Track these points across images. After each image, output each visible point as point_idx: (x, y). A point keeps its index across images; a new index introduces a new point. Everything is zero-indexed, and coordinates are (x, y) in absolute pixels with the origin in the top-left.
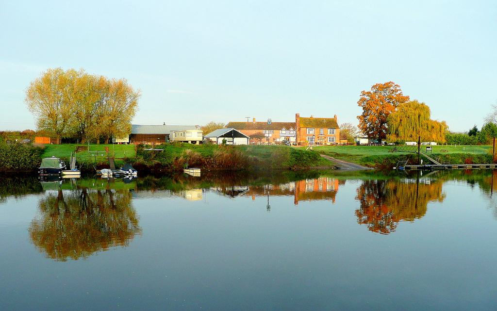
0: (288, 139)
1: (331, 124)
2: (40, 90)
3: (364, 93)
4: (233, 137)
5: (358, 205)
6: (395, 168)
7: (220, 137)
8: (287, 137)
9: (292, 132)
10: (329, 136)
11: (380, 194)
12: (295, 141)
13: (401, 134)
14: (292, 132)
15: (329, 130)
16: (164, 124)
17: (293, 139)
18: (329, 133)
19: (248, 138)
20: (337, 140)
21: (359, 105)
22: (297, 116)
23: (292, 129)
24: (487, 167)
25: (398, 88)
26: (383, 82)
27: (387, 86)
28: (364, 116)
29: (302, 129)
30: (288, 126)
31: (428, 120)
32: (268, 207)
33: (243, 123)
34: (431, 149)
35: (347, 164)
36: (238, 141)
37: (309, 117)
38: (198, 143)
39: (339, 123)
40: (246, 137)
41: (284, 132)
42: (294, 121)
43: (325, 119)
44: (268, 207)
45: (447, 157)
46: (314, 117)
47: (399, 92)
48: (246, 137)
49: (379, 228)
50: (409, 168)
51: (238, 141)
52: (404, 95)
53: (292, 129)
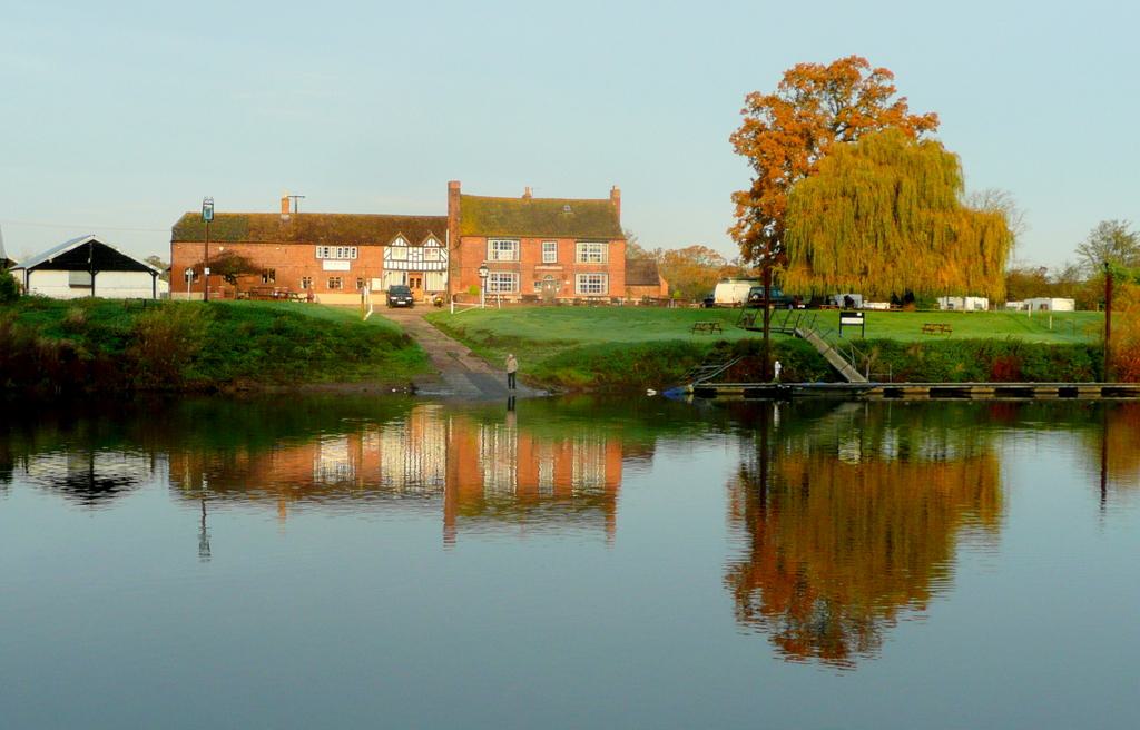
0: (416, 278)
1: (597, 221)
2: (1117, 234)
3: (757, 102)
4: (94, 269)
5: (734, 545)
7: (45, 266)
8: (412, 272)
9: (431, 260)
11: (504, 507)
12: (443, 288)
13: (824, 261)
14: (434, 256)
17: (436, 283)
19: (155, 274)
20: (609, 288)
21: (731, 140)
22: (453, 191)
23: (431, 242)
24: (1063, 392)
25: (886, 83)
26: (825, 58)
27: (840, 77)
28: (756, 193)
29: (468, 243)
30: (416, 230)
31: (948, 206)
32: (204, 545)
33: (238, 216)
34: (860, 321)
35: (731, 394)
36: (112, 286)
37: (518, 194)
43: (572, 203)
44: (204, 545)
45: (911, 352)
46: (537, 194)
47: (891, 101)
49: (833, 648)
50: (710, 393)
51: (112, 286)
52: (916, 109)
53: (431, 242)
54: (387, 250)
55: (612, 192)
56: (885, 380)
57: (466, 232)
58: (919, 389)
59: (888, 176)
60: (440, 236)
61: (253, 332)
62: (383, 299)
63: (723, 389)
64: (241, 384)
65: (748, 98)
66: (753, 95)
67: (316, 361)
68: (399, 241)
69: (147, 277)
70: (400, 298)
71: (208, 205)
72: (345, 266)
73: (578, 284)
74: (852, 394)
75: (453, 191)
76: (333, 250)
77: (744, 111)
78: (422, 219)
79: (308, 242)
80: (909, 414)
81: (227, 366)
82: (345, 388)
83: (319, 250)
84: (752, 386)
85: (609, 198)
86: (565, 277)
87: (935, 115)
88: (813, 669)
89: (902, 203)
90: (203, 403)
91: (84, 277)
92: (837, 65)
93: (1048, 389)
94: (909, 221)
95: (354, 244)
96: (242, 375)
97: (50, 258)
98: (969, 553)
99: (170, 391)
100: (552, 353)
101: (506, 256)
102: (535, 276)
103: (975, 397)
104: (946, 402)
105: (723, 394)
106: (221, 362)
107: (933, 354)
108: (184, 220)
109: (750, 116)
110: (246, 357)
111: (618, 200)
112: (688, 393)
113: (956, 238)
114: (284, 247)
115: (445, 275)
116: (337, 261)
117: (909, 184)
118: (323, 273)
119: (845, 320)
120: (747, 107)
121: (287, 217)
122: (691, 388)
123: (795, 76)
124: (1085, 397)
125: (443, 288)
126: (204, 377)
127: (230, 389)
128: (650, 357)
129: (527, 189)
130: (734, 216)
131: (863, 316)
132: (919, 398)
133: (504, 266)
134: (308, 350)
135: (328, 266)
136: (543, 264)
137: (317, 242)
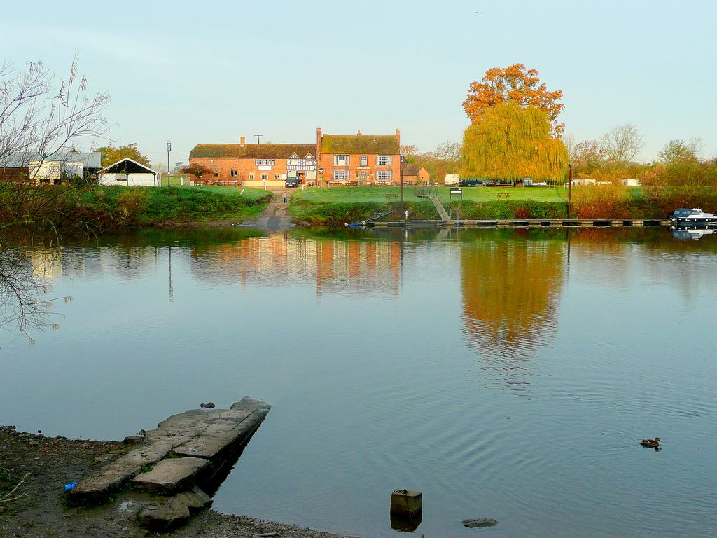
1: (387, 146)
3: (476, 87)
6: (346, 225)
9: (309, 164)
10: (379, 169)
12: (315, 178)
14: (310, 163)
15: (378, 158)
16: (74, 151)
18: (378, 163)
19: (155, 174)
22: (319, 133)
23: (309, 157)
24: (543, 224)
26: (504, 65)
27: (513, 73)
35: (381, 225)
36: (135, 180)
37: (355, 133)
38: (52, 183)
39: (403, 143)
40: (152, 173)
41: (294, 162)
42: (314, 142)
43: (376, 137)
46: (364, 133)
47: (538, 85)
48: (152, 173)
50: (372, 225)
52: (551, 90)
54: (288, 161)
56: (541, 217)
57: (323, 152)
58: (472, 223)
59: (504, 123)
60: (313, 154)
61: (179, 200)
62: (283, 184)
63: (378, 223)
64: (167, 222)
65: (471, 85)
66: (473, 83)
67: (205, 213)
70: (294, 183)
72: (269, 168)
73: (378, 175)
74: (444, 225)
76: (264, 161)
77: (469, 91)
78: (306, 146)
79: (252, 158)
80: (525, 233)
81: (162, 215)
82: (214, 224)
83: (257, 161)
84: (646, 220)
85: (395, 134)
86: (371, 172)
87: (560, 92)
90: (150, 230)
91: (123, 176)
92: (511, 69)
93: (557, 223)
94: (515, 144)
95: (273, 158)
96: (169, 218)
99: (133, 225)
100: (315, 208)
101: (342, 163)
102: (357, 172)
103: (499, 226)
104: (568, 228)
105: (377, 225)
106: (160, 213)
107: (487, 207)
108: (195, 148)
109: (472, 93)
110: (173, 211)
111: (399, 136)
112: (362, 225)
113: (536, 153)
114: (240, 160)
115: (316, 172)
116: (265, 167)
117: (514, 127)
118: (259, 172)
119: (452, 192)
120: (470, 89)
121: (243, 146)
122: (364, 223)
123: (491, 74)
124: (554, 226)
125: (315, 178)
126: (149, 219)
127: (161, 225)
128: (355, 209)
129: (359, 131)
130: (563, 125)
131: (461, 190)
132: (472, 227)
133: (341, 167)
134: (203, 208)
135: (261, 168)
136: (360, 166)
137: (256, 157)
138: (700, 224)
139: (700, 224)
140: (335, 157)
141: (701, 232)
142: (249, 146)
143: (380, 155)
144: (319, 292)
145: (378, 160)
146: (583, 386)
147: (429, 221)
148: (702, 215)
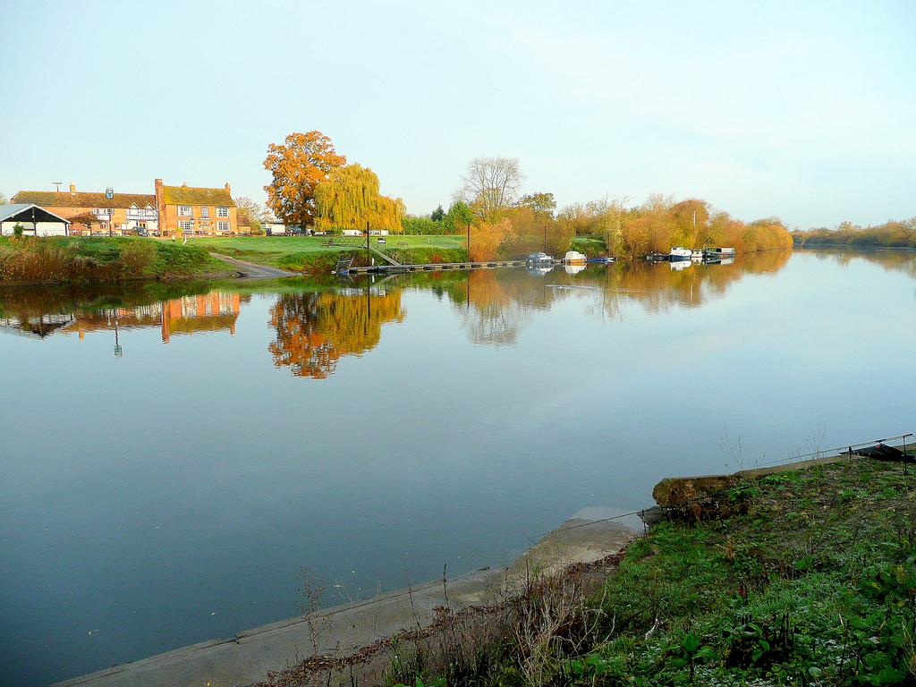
1: (221, 198)
3: (273, 148)
4: (35, 221)
8: (140, 221)
9: (149, 213)
10: (219, 219)
11: (308, 315)
13: (338, 218)
14: (150, 213)
15: (218, 210)
18: (218, 214)
22: (158, 183)
24: (461, 267)
25: (328, 143)
27: (309, 138)
30: (141, 202)
31: (376, 195)
36: (44, 229)
37: (179, 184)
47: (329, 149)
55: (226, 186)
59: (360, 183)
68: (133, 207)
69: (62, 225)
71: (843, 262)
75: (158, 183)
85: (224, 188)
87: (156, 180)
88: (308, 380)
89: (365, 193)
97: (13, 216)
98: (387, 329)
138: (545, 264)
139: (545, 264)
140: (179, 208)
141: (545, 270)
142: (81, 195)
143: (220, 207)
144: (165, 338)
145: (218, 212)
146: (860, 445)
147: (266, 267)
148: (546, 258)
